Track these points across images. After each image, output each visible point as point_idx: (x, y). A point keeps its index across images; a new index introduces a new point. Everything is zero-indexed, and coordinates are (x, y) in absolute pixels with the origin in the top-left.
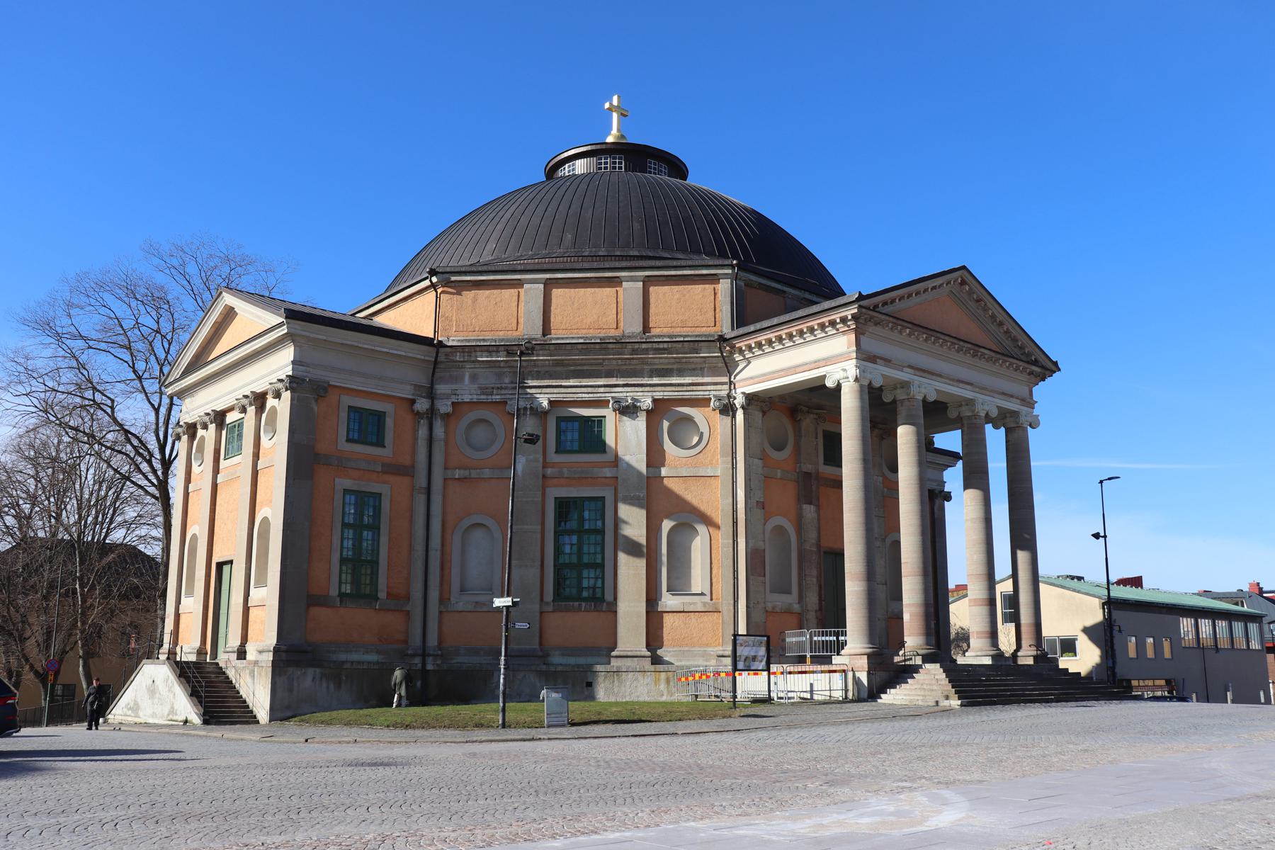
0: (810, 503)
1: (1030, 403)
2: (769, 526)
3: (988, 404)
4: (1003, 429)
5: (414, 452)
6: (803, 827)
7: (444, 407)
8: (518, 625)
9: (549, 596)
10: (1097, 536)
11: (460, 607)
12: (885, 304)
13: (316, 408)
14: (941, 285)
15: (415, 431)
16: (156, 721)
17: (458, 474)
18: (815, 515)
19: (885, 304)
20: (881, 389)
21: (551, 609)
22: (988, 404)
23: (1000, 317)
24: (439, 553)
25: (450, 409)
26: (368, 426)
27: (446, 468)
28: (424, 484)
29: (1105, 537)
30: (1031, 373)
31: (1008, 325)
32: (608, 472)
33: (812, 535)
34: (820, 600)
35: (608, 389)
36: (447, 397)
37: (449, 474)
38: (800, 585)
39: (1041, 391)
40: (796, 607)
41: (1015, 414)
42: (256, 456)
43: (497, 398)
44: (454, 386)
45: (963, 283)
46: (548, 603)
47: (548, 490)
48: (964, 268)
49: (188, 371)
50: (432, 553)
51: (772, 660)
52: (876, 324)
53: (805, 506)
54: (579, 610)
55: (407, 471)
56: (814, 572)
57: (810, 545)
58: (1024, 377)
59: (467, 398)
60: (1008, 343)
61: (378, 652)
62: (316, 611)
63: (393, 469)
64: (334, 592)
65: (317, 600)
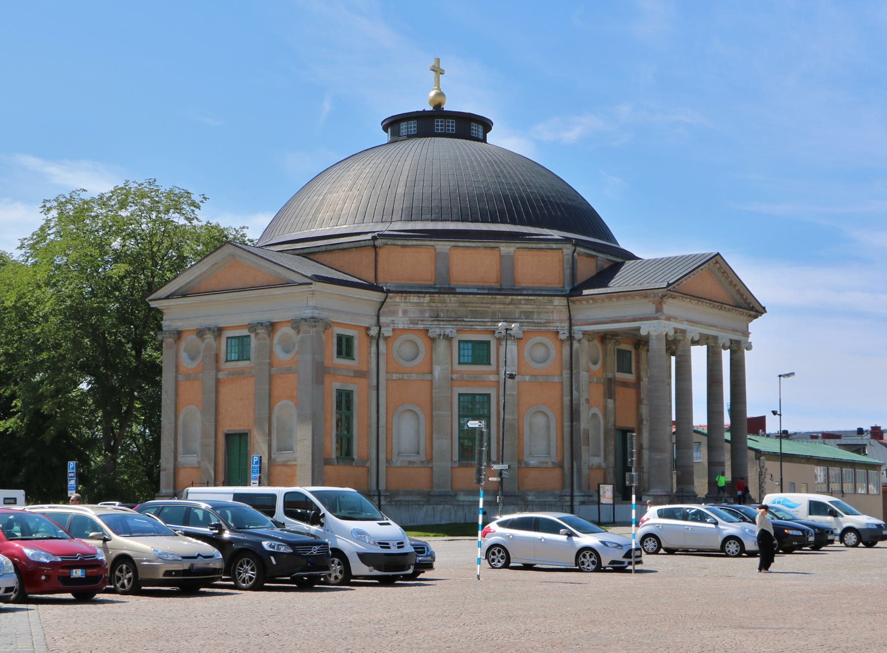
1: (746, 334)
3: (725, 337)
7: (387, 332)
8: (495, 479)
9: (456, 458)
11: (398, 464)
13: (324, 338)
16: (190, 539)
17: (395, 376)
21: (457, 465)
28: (375, 383)
29: (780, 415)
30: (750, 316)
32: (493, 378)
33: (611, 419)
36: (388, 325)
38: (605, 451)
39: (754, 326)
40: (603, 465)
43: (421, 327)
44: (392, 318)
46: (455, 462)
47: (454, 388)
51: (844, 481)
53: (609, 400)
56: (613, 443)
57: (610, 426)
58: (746, 318)
59: (401, 327)
60: (738, 297)
63: (361, 374)
65: (327, 462)
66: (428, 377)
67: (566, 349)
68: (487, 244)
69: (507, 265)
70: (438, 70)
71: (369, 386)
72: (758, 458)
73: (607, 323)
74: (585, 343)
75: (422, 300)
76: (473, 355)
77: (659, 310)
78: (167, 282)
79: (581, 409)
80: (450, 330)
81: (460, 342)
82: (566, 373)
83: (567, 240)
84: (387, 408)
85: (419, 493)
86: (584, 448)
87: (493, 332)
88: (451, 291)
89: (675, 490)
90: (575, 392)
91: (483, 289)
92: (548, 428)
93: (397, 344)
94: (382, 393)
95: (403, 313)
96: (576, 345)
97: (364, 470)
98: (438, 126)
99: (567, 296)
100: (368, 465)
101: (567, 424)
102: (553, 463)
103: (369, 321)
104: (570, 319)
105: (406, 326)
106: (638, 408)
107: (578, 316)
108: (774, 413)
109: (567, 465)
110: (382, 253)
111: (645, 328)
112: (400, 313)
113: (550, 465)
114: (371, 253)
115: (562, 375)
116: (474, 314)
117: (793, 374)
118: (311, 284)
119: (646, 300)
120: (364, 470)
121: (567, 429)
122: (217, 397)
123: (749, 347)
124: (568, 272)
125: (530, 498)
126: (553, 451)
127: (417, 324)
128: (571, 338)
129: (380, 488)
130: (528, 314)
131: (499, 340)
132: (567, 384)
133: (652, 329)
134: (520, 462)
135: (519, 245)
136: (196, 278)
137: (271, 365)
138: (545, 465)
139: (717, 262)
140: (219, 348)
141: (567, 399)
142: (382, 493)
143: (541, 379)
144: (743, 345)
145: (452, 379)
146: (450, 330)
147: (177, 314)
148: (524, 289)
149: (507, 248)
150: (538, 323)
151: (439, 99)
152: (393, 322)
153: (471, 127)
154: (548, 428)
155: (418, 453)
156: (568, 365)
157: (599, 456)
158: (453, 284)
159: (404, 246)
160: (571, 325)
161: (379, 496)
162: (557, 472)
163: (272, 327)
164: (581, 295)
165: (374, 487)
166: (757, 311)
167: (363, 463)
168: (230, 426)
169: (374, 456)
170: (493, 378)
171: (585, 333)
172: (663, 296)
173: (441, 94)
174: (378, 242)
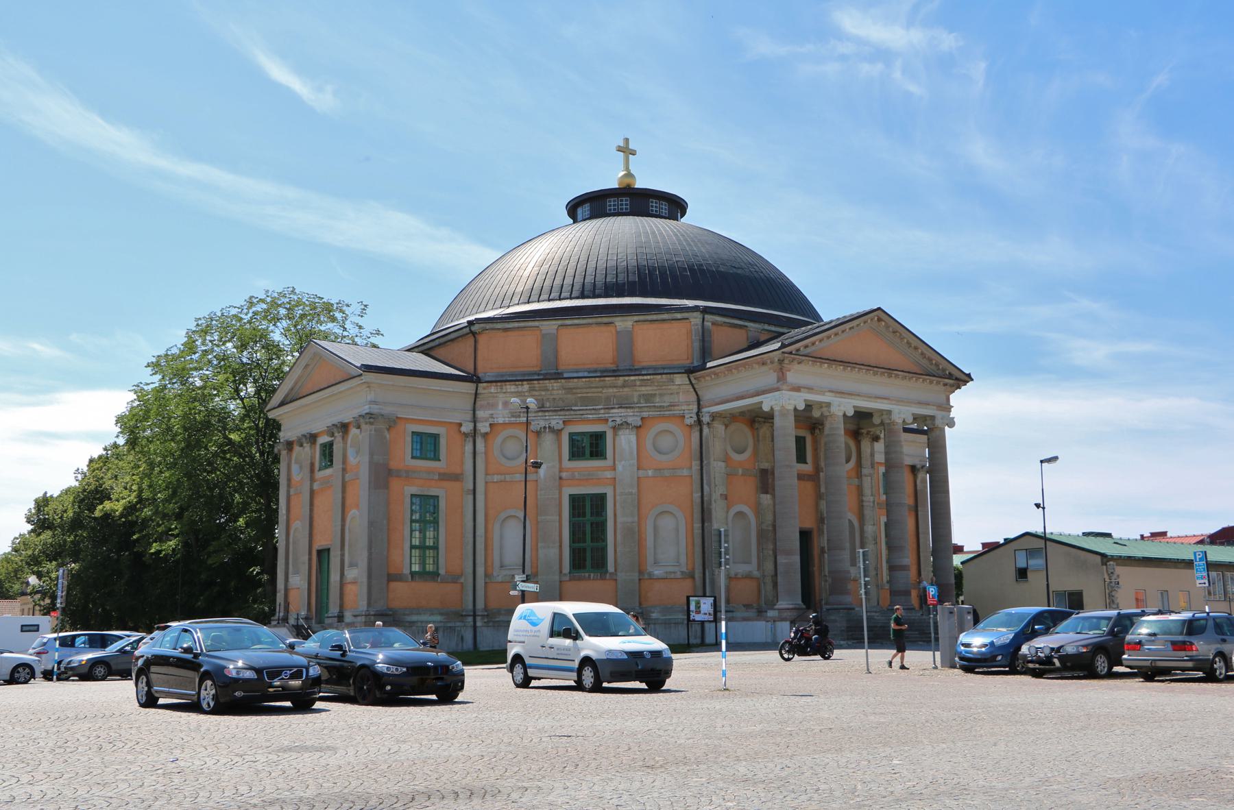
1: (948, 408)
3: (902, 414)
5: (462, 463)
7: (483, 427)
10: (1038, 506)
11: (499, 579)
15: (463, 446)
17: (496, 478)
18: (771, 502)
19: (806, 347)
21: (567, 578)
22: (902, 414)
23: (915, 343)
25: (488, 429)
26: (427, 445)
28: (471, 487)
31: (923, 348)
32: (609, 474)
40: (756, 573)
42: (344, 470)
48: (879, 309)
49: (282, 404)
50: (478, 539)
58: (941, 387)
59: (501, 420)
60: (924, 362)
61: (441, 614)
62: (393, 585)
64: (406, 571)
67: (696, 435)
68: (599, 320)
69: (626, 342)
70: (626, 150)
72: (1104, 563)
74: (719, 427)
75: (520, 389)
77: (782, 378)
78: (274, 391)
80: (556, 422)
82: (696, 465)
83: (696, 308)
84: (486, 515)
87: (606, 420)
88: (558, 376)
90: (705, 487)
91: (596, 371)
92: (677, 530)
93: (499, 439)
95: (504, 404)
96: (706, 430)
99: (690, 371)
100: (462, 580)
101: (698, 525)
102: (682, 572)
103: (463, 417)
104: (699, 400)
106: (817, 505)
107: (707, 396)
108: (1038, 506)
109: (698, 575)
110: (482, 340)
111: (767, 403)
112: (500, 406)
113: (679, 575)
114: (471, 340)
115: (691, 468)
116: (586, 401)
117: (1056, 458)
119: (765, 368)
121: (698, 531)
122: (311, 510)
123: (951, 424)
124: (697, 345)
125: (654, 616)
126: (683, 559)
130: (648, 398)
131: (614, 428)
132: (696, 477)
134: (641, 572)
135: (636, 318)
136: (296, 383)
139: (879, 320)
140: (313, 457)
142: (478, 613)
143: (667, 473)
144: (938, 422)
145: (561, 478)
146: (556, 422)
147: (294, 422)
148: (643, 368)
149: (623, 323)
151: (628, 181)
152: (492, 416)
153: (675, 206)
154: (677, 530)
157: (749, 563)
158: (561, 368)
159: (506, 330)
161: (475, 616)
163: (344, 427)
165: (471, 607)
166: (957, 379)
167: (454, 579)
168: (320, 543)
170: (609, 474)
171: (714, 416)
172: (781, 361)
173: (629, 175)
174: (475, 328)
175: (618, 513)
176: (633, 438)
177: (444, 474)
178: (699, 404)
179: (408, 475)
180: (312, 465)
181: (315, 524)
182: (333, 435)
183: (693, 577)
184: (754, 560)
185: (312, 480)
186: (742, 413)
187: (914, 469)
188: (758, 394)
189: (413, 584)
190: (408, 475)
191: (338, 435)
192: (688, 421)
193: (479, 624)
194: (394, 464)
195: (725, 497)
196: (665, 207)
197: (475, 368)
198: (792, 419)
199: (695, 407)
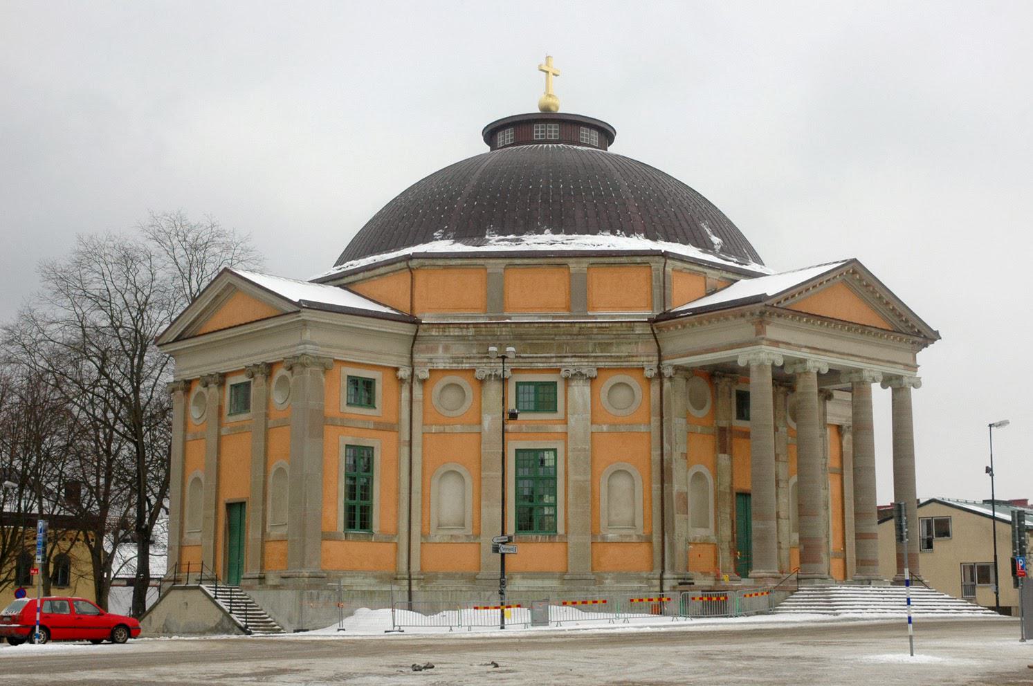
0: (725, 453)
1: (915, 368)
2: (691, 473)
4: (890, 389)
5: (398, 412)
6: (250, 288)
7: (423, 373)
12: (786, 299)
13: (324, 380)
14: (835, 277)
18: (728, 462)
19: (786, 299)
20: (782, 367)
24: (420, 495)
27: (424, 424)
28: (407, 438)
32: (559, 428)
34: (733, 533)
35: (559, 360)
37: (427, 429)
39: (925, 357)
40: (713, 538)
41: (899, 378)
43: (466, 366)
45: (854, 272)
52: (779, 316)
54: (536, 541)
55: (392, 428)
56: (728, 510)
58: (909, 346)
59: (441, 367)
61: (375, 577)
62: (327, 544)
63: (380, 427)
66: (476, 429)
67: (655, 388)
71: (399, 441)
73: (701, 353)
74: (680, 382)
76: (536, 401)
79: (674, 466)
81: (518, 384)
82: (655, 420)
84: (423, 469)
85: (462, 576)
86: (678, 518)
87: (559, 370)
89: (1019, 619)
93: (437, 388)
94: (417, 450)
96: (667, 384)
97: (391, 547)
98: (555, 132)
101: (656, 486)
102: (639, 536)
104: (659, 351)
105: (448, 366)
107: (668, 347)
109: (656, 539)
110: (420, 277)
111: (743, 357)
112: (440, 349)
113: (634, 539)
115: (650, 423)
118: (299, 312)
119: (743, 320)
120: (391, 547)
121: (656, 493)
122: (218, 459)
123: (917, 384)
126: (639, 522)
127: (462, 363)
128: (660, 375)
129: (413, 570)
131: (567, 379)
133: (752, 356)
134: (593, 535)
137: (267, 415)
138: (627, 540)
140: (221, 399)
141: (656, 454)
150: (618, 357)
155: (463, 525)
156: (658, 410)
160: (660, 361)
161: (410, 579)
162: (645, 547)
163: (270, 368)
164: (648, 319)
165: (404, 568)
167: (389, 538)
169: (404, 529)
170: (559, 428)
171: (677, 368)
175: (571, 469)
176: (587, 390)
177: (379, 423)
178: (660, 356)
179: (343, 423)
180: (220, 408)
181: (223, 474)
182: (252, 376)
183: (649, 541)
184: (712, 525)
185: (220, 425)
186: (703, 367)
187: (839, 428)
188: (732, 346)
189: (346, 543)
190: (343, 423)
191: (260, 378)
192: (648, 373)
193: (414, 588)
194: (330, 411)
195: (685, 456)
196: (595, 136)
197: (412, 308)
198: (770, 375)
199: (656, 358)
